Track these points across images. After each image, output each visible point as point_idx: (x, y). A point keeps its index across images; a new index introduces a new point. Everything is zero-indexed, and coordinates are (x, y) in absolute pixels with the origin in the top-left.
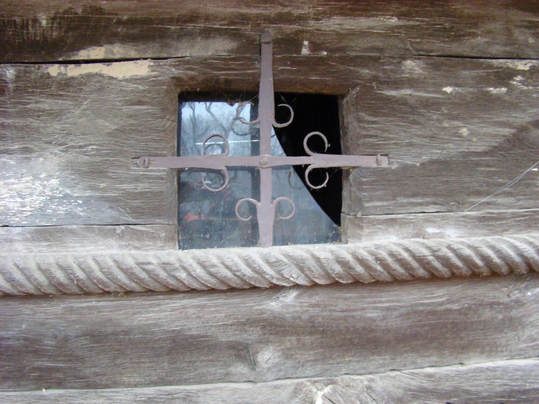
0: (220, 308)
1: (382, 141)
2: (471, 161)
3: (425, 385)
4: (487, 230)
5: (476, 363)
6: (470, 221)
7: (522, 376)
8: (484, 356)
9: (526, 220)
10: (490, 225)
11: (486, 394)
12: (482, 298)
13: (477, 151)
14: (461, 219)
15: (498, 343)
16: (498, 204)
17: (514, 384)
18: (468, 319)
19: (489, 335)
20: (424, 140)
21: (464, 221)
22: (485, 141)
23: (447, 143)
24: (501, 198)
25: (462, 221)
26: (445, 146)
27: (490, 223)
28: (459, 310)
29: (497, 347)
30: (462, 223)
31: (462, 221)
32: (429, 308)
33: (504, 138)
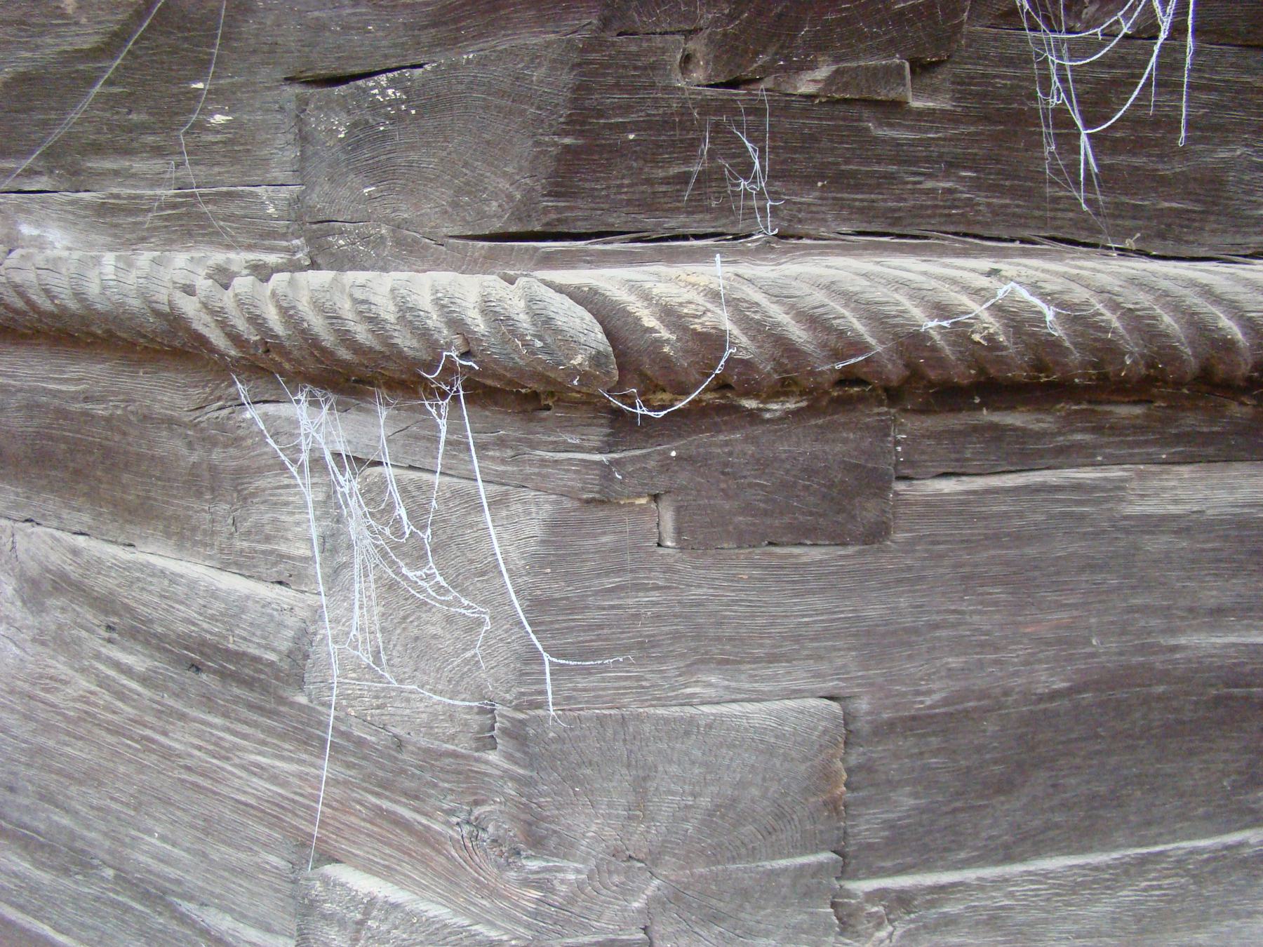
0: (1104, 597)
1: (856, 200)
2: (77, 71)
3: (68, 568)
4: (110, 235)
5: (157, 556)
6: (82, 213)
7: (222, 614)
8: (171, 542)
9: (180, 217)
10: (116, 226)
11: (160, 630)
12: (148, 402)
13: (85, 46)
14: (69, 208)
15: (194, 522)
16: (133, 176)
17: (205, 626)
18: (129, 444)
19: (175, 497)
20: (9, 30)
21: (74, 214)
22: (99, 23)
23: (41, 34)
24: (142, 160)
25: (69, 212)
26: (39, 41)
27: (115, 220)
28: (108, 420)
29: (194, 529)
30: (71, 217)
31: (69, 212)
32: (56, 402)
33: (131, 11)
